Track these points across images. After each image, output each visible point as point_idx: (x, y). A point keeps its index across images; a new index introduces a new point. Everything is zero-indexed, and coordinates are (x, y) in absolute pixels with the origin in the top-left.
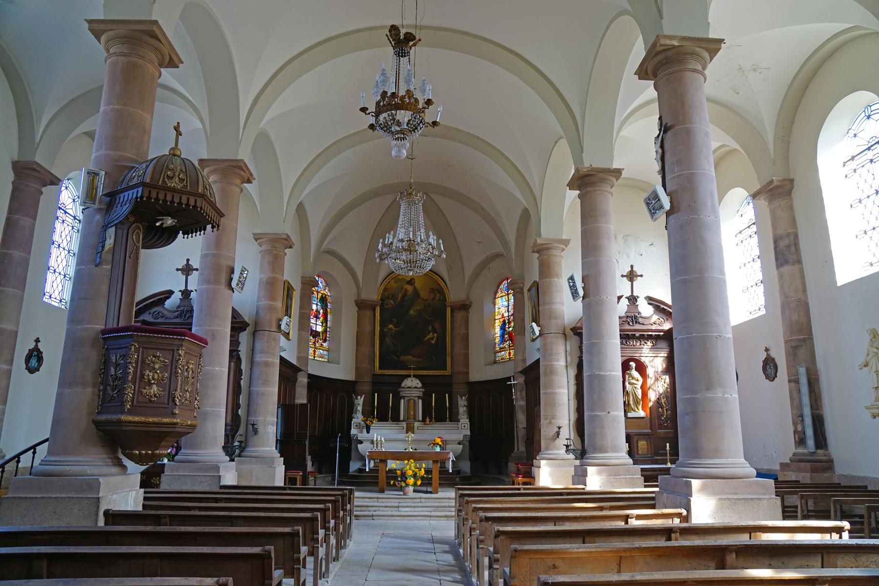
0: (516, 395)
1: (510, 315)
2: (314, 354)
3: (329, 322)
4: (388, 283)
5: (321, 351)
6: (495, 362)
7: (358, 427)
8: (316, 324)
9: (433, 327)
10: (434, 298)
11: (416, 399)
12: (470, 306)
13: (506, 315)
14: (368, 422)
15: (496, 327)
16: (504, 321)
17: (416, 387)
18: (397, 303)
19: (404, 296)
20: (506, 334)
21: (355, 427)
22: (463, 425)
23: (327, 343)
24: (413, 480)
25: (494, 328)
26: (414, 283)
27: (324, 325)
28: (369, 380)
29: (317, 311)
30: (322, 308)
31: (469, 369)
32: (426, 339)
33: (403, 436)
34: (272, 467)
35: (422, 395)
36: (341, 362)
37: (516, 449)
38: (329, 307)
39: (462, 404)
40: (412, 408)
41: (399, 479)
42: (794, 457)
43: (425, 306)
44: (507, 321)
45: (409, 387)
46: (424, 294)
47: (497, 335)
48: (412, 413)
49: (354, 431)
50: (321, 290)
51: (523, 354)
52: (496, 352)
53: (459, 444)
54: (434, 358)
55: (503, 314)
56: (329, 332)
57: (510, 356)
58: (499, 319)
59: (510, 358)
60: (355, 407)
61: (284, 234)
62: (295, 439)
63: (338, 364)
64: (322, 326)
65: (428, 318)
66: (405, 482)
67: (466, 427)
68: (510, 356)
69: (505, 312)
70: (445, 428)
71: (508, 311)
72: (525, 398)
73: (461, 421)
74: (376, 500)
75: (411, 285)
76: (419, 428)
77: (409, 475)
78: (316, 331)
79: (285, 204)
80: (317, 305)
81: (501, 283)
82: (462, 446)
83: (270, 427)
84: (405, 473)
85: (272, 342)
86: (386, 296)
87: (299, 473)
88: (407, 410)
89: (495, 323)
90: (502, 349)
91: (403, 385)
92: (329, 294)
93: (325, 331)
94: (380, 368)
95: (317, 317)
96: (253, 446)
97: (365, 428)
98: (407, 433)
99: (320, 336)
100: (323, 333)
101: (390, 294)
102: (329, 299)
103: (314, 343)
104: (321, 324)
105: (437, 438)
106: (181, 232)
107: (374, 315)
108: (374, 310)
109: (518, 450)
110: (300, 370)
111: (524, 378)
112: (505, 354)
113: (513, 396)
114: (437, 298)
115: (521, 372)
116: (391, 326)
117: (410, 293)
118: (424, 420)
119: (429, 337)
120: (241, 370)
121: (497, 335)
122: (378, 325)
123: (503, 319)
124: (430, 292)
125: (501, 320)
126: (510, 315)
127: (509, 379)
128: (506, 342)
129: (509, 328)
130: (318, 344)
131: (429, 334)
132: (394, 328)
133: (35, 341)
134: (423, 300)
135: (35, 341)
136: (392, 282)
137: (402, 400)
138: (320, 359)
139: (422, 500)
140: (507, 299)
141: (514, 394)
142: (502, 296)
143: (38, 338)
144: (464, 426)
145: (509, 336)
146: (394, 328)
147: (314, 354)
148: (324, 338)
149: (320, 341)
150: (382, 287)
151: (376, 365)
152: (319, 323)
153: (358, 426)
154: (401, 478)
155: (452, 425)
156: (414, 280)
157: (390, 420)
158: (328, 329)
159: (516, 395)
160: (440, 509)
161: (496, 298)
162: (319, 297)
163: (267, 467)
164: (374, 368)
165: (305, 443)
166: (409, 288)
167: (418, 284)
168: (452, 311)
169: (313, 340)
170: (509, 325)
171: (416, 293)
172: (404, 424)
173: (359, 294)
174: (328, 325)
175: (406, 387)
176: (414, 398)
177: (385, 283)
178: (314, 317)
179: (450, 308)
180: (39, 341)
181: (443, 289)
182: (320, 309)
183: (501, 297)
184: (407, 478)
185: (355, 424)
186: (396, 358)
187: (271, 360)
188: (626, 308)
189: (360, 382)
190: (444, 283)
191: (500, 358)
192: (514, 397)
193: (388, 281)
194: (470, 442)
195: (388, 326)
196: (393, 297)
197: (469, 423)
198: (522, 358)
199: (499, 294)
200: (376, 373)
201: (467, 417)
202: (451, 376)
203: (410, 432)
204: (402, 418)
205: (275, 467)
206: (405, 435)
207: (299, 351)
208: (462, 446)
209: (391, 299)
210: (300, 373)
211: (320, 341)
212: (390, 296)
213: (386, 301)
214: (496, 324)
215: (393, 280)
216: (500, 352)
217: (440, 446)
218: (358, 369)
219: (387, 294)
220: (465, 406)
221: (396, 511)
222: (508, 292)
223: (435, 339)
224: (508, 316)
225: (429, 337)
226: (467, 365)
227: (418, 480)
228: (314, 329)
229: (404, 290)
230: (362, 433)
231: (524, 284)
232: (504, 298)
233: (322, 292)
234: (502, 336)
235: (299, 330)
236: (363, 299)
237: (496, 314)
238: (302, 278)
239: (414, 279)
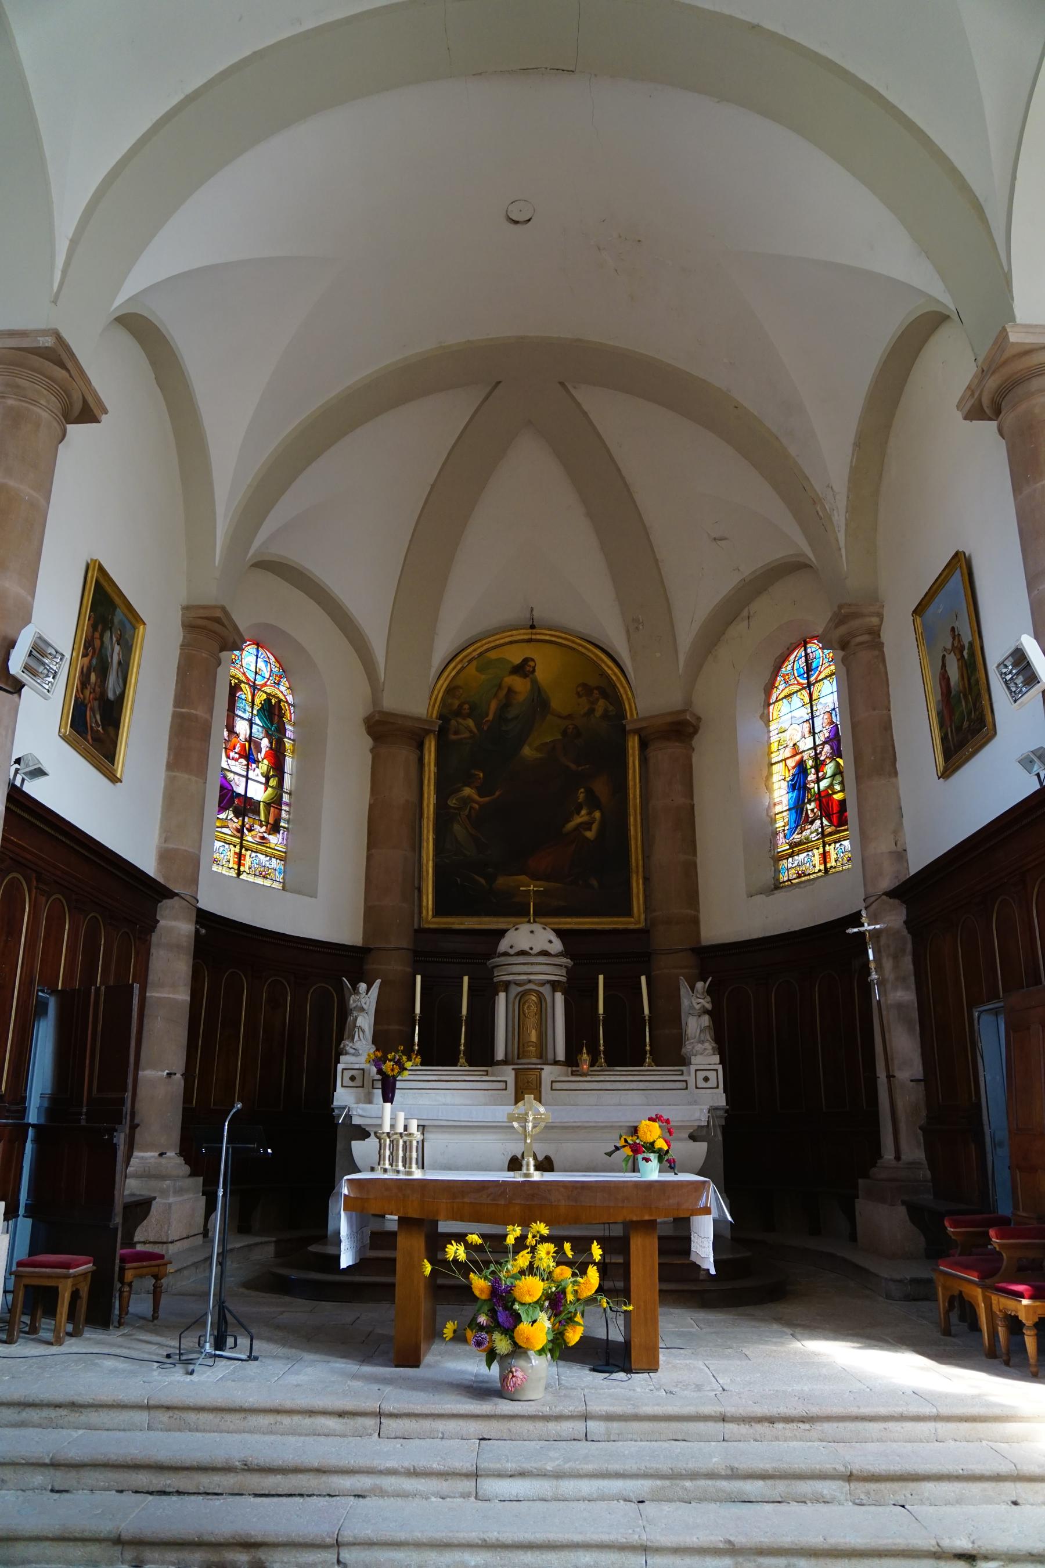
0: (879, 968)
1: (818, 742)
2: (239, 864)
3: (287, 779)
4: (458, 673)
5: (262, 857)
6: (777, 886)
7: (358, 1082)
8: (247, 778)
9: (590, 792)
10: (592, 711)
11: (546, 990)
12: (696, 730)
13: (808, 743)
14: (387, 1067)
15: (776, 786)
16: (801, 764)
17: (544, 953)
18: (485, 728)
19: (505, 706)
20: (809, 802)
21: (347, 1081)
22: (701, 1075)
23: (280, 836)
24: (548, 1324)
25: (769, 788)
26: (534, 671)
27: (273, 782)
28: (404, 944)
29: (250, 739)
30: (268, 735)
31: (698, 911)
32: (571, 825)
33: (501, 1112)
35: (564, 979)
36: (322, 889)
37: (888, 1154)
38: (289, 734)
39: (697, 1007)
40: (532, 1020)
41: (483, 1319)
43: (564, 733)
44: (810, 763)
45: (523, 953)
46: (560, 701)
47: (778, 809)
48: (533, 1036)
49: (343, 1096)
50: (265, 685)
51: (895, 832)
52: (779, 858)
53: (693, 1137)
54: (595, 883)
55: (795, 745)
56: (287, 804)
57: (825, 863)
58: (785, 760)
59: (826, 870)
60: (350, 1019)
61: (44, 332)
62: (83, 1123)
63: (313, 895)
64: (267, 784)
65: (573, 766)
66: (509, 1331)
67: (712, 1082)
68: (825, 863)
69: (804, 737)
70: (642, 1085)
71: (813, 733)
72: (912, 978)
73: (694, 1060)
74: (371, 1422)
75: (526, 676)
76: (556, 1086)
77: (528, 1299)
78: (246, 799)
79: (62, 248)
80: (251, 723)
81: (784, 659)
82: (703, 1146)
84: (510, 1289)
86: (455, 707)
87: (68, 1266)
88: (517, 1028)
89: (770, 774)
90: (795, 848)
91: (503, 946)
92: (290, 698)
93: (276, 802)
94: (438, 911)
95: (249, 757)
97: (379, 1085)
98: (518, 1099)
99: (259, 814)
100: (268, 805)
101: (464, 703)
102: (289, 714)
103: (240, 831)
104: (263, 780)
105: (645, 1124)
106: (713, 1272)
107: (421, 760)
108: (420, 746)
109: (898, 1158)
110: (171, 894)
111: (904, 911)
112: (811, 861)
113: (869, 974)
114: (599, 712)
115: (891, 894)
116: (467, 791)
117: (521, 698)
118: (571, 1061)
119: (578, 820)
121: (778, 809)
122: (432, 788)
123: (798, 757)
124: (579, 695)
125: (791, 763)
126: (818, 742)
127: (855, 919)
128: (812, 823)
129: (818, 780)
130: (254, 837)
131: (578, 813)
132: (476, 797)
134: (560, 717)
136: (472, 669)
137: (502, 996)
138: (259, 881)
139: (591, 1424)
140: (807, 699)
141: (872, 966)
142: (790, 695)
144: (706, 1079)
145: (820, 807)
146: (476, 797)
147: (239, 864)
148: (271, 821)
149: (257, 827)
150: (443, 684)
151: (424, 904)
152: (257, 773)
153: (358, 1080)
154: (493, 1314)
155: (665, 1074)
156: (532, 664)
157: (462, 1061)
158: (286, 798)
159: (879, 968)
160: (688, 1484)
161: (770, 704)
162: (257, 701)
164: (420, 913)
165: (112, 1137)
166: (520, 685)
167: (542, 674)
168: (644, 745)
169: (237, 823)
170: (817, 772)
171: (539, 701)
172: (508, 1074)
173: (376, 699)
174: (287, 784)
175: (512, 952)
176: (541, 989)
177: (451, 672)
178: (241, 756)
179: (636, 739)
181: (614, 686)
182: (261, 736)
183: (785, 697)
184: (517, 1319)
185: (348, 1074)
186: (483, 881)
189: (379, 949)
190: (616, 670)
191: (793, 873)
192: (874, 976)
193: (460, 666)
194: (725, 1130)
195: (460, 790)
196: (475, 711)
197: (720, 1068)
198: (893, 848)
199: (781, 689)
200: (426, 926)
201: (713, 1048)
202: (645, 932)
203: (529, 1097)
204: (500, 1054)
206: (511, 1109)
207: (168, 832)
208: (703, 1146)
209: (469, 716)
210: (167, 903)
211: (257, 827)
212: (466, 706)
213: (453, 722)
214: (776, 778)
215: (475, 663)
216: (792, 855)
217: (661, 1155)
218: (372, 914)
219: (457, 703)
220: (706, 1012)
221: (465, 1496)
222: (808, 678)
223: (595, 827)
224: (815, 748)
225: (578, 820)
226: (692, 897)
227: (570, 1320)
228: (240, 790)
229: (504, 692)
230: (370, 1102)
231: (880, 616)
232: (796, 700)
233: (268, 689)
234: (798, 808)
235: (170, 767)
236: (384, 710)
237: (774, 747)
238: (186, 608)
239: (533, 660)
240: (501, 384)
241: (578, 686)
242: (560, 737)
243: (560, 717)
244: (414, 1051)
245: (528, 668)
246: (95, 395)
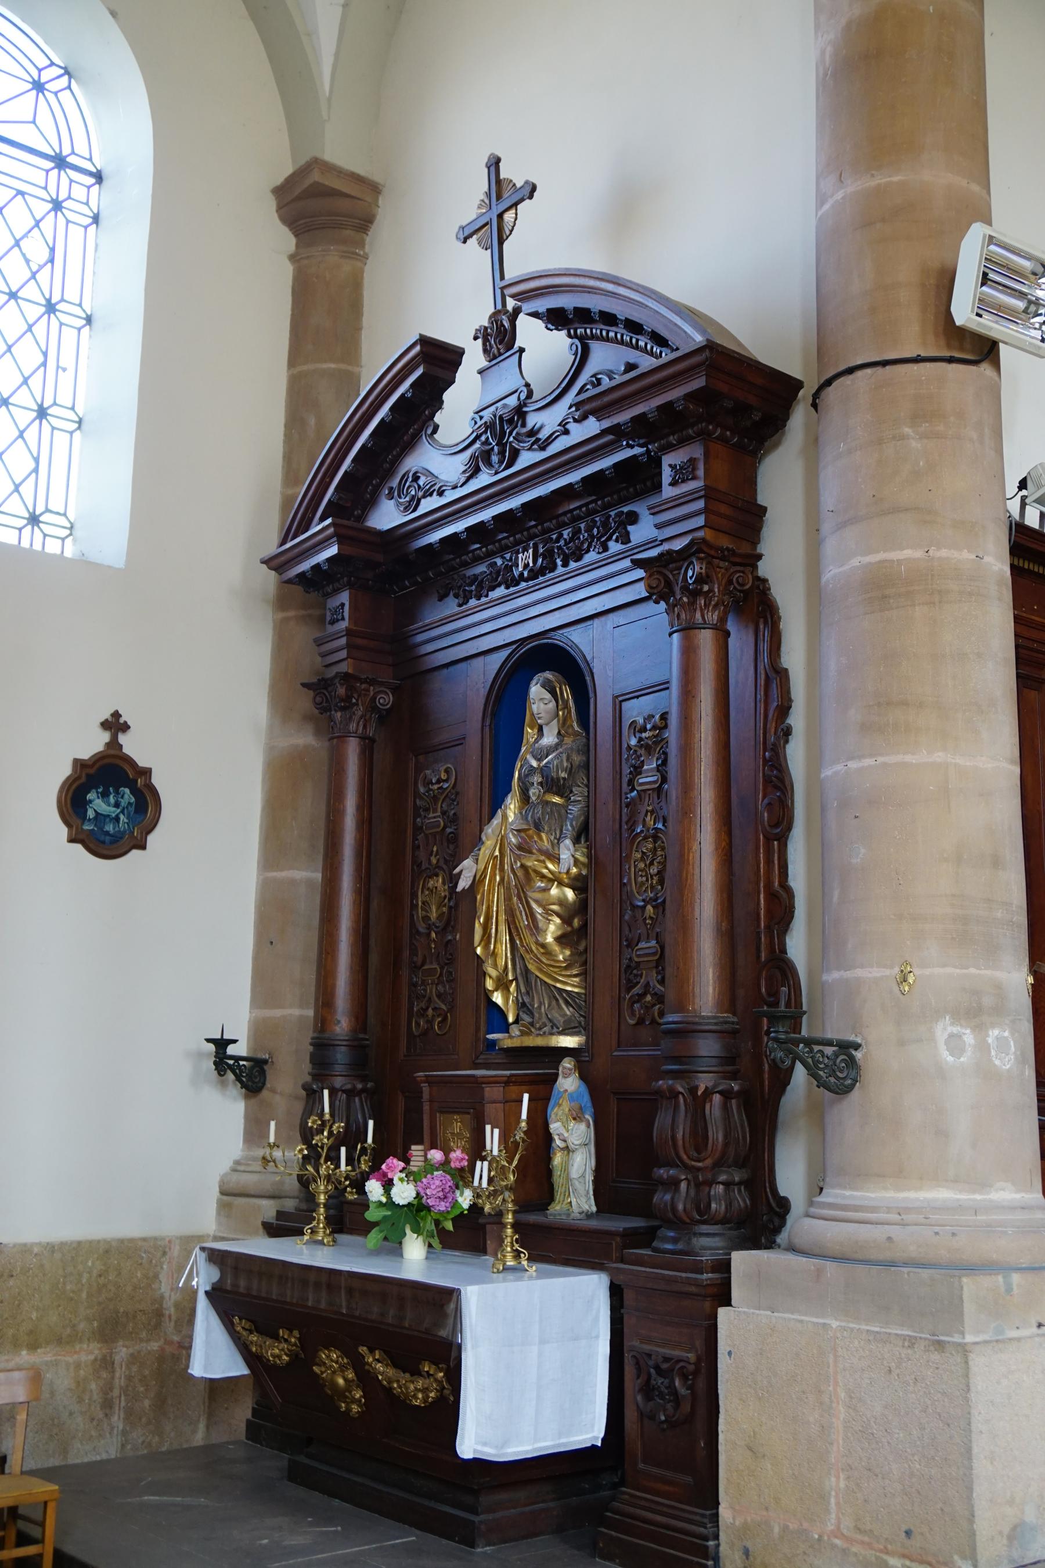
34: (940, 1346)
42: (235, 1177)
83: (944, 1029)
85: (907, 430)
96: (860, 1176)
120: (783, 675)
133: (105, 725)
135: (105, 725)
143: (116, 715)
163: (911, 1342)
180: (125, 727)
187: (907, 553)
205: (964, 1350)
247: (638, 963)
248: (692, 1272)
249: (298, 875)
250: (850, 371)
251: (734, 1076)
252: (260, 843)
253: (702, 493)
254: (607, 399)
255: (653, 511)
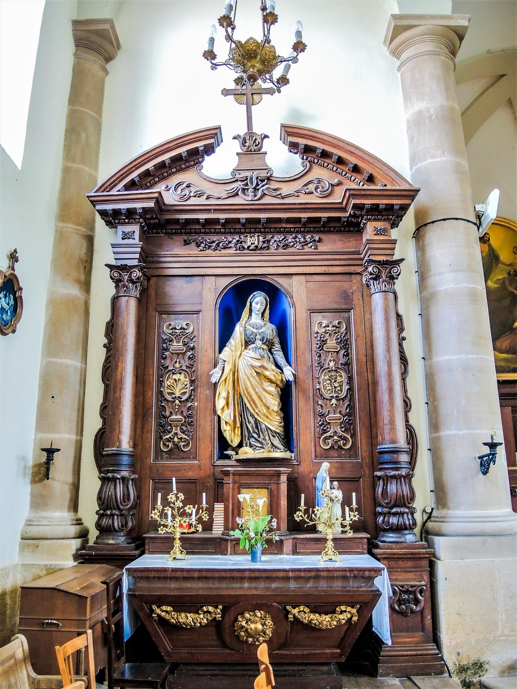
26: (489, 240)
43: (509, 274)
134: (506, 265)
156: (487, 236)
188: (234, 162)
239: (488, 234)
240: (505, 77)
241: (513, 249)
242: (507, 276)
243: (506, 265)
244: (269, 642)
245: (486, 238)
246: (116, 37)
247: (329, 423)
248: (405, 549)
249: (446, 358)
250: (433, 222)
251: (134, 472)
252: (43, 341)
253: (141, 246)
254: (363, 192)
255: (113, 246)
